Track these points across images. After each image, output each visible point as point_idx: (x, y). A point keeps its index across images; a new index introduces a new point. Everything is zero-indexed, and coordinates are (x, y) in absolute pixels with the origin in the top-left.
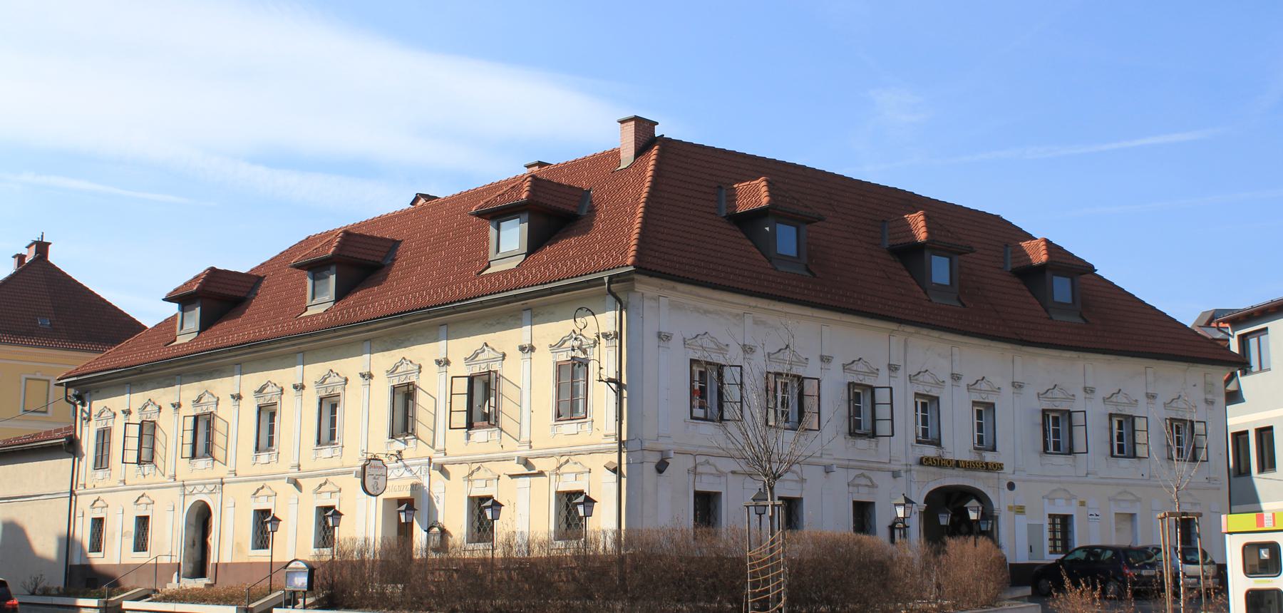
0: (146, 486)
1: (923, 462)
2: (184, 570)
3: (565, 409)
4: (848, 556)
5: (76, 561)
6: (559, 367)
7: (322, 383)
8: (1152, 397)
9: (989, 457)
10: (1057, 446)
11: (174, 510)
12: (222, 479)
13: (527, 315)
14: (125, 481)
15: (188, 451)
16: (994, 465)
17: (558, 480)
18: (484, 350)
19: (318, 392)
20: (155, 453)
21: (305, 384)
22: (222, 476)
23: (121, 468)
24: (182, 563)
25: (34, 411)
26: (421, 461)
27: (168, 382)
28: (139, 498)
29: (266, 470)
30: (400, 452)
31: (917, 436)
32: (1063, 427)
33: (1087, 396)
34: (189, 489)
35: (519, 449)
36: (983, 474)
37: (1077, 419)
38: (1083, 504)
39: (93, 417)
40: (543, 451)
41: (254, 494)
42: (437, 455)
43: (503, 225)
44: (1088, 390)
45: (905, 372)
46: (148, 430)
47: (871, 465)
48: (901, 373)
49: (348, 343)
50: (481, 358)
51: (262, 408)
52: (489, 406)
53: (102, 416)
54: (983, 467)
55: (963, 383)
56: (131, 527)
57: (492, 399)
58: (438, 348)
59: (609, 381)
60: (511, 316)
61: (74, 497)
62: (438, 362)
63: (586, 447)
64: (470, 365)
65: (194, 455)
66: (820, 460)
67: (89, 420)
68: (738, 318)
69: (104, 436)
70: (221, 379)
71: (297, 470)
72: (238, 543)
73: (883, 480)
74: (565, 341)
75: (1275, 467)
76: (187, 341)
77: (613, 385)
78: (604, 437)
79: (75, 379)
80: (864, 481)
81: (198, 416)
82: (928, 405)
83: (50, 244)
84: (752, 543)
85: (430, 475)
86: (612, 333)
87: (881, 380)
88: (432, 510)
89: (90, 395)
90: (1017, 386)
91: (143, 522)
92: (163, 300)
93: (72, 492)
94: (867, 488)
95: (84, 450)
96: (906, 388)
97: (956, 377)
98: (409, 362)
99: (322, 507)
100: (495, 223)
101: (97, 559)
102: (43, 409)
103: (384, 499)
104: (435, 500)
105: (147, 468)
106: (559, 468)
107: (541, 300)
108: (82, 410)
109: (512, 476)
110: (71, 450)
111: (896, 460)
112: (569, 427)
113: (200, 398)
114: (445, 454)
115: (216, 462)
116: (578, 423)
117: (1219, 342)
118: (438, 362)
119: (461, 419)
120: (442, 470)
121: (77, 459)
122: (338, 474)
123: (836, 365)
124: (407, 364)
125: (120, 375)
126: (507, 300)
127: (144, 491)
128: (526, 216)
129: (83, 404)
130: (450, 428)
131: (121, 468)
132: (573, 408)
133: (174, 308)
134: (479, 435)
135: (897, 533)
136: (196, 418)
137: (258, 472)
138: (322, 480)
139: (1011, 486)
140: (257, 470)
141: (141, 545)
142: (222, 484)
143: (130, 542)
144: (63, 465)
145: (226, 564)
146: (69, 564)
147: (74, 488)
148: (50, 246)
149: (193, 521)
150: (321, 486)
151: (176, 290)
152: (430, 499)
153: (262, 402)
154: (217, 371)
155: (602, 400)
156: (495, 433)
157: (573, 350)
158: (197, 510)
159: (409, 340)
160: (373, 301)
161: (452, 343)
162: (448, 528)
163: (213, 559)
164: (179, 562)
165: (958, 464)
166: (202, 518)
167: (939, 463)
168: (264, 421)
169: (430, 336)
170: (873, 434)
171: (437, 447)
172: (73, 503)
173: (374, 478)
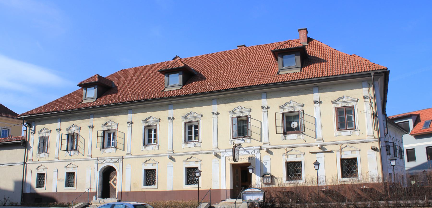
0: (73, 160)
2: (99, 195)
4: (296, 186)
5: (28, 191)
7: (186, 117)
11: (91, 170)
12: (123, 157)
13: (316, 89)
14: (58, 158)
15: (100, 145)
17: (341, 154)
18: (291, 103)
19: (39, 135)
20: (78, 147)
21: (61, 129)
22: (123, 155)
24: (98, 192)
26: (254, 148)
27: (85, 117)
28: (68, 165)
29: (151, 153)
34: (100, 161)
35: (316, 142)
39: (36, 132)
40: (332, 142)
41: (144, 163)
42: (264, 145)
43: (88, 89)
49: (202, 100)
50: (289, 106)
51: (146, 127)
53: (42, 131)
58: (57, 125)
60: (306, 89)
61: (25, 165)
62: (57, 130)
63: (357, 141)
64: (231, 114)
65: (103, 147)
67: (35, 133)
70: (119, 116)
71: (172, 152)
72: (134, 184)
74: (340, 99)
75: (416, 160)
76: (93, 101)
79: (29, 116)
81: (105, 131)
84: (395, 179)
85: (260, 153)
86: (216, 112)
88: (262, 166)
89: (35, 123)
92: (77, 85)
93: (25, 163)
95: (31, 145)
98: (76, 126)
99: (39, 173)
100: (167, 75)
101: (40, 190)
104: (264, 164)
105: (73, 153)
106: (341, 149)
107: (323, 83)
108: (30, 130)
109: (312, 153)
110: (25, 145)
113: (106, 123)
114: (270, 145)
115: (305, 135)
116: (351, 131)
117: (398, 124)
118: (57, 130)
120: (268, 151)
121: (27, 149)
122: (199, 154)
124: (46, 130)
125: (38, 117)
126: (319, 81)
127: (42, 164)
128: (96, 86)
129: (31, 127)
130: (61, 150)
133: (79, 88)
137: (146, 154)
138: (190, 156)
140: (145, 152)
142: (123, 158)
144: (21, 152)
145: (128, 192)
146: (23, 192)
147: (25, 161)
150: (188, 159)
151: (83, 82)
152: (261, 164)
154: (116, 112)
156: (301, 136)
158: (104, 169)
159: (242, 99)
160: (109, 99)
161: (321, 94)
162: (273, 174)
164: (96, 191)
168: (146, 133)
169: (126, 112)
171: (263, 141)
172: (25, 167)
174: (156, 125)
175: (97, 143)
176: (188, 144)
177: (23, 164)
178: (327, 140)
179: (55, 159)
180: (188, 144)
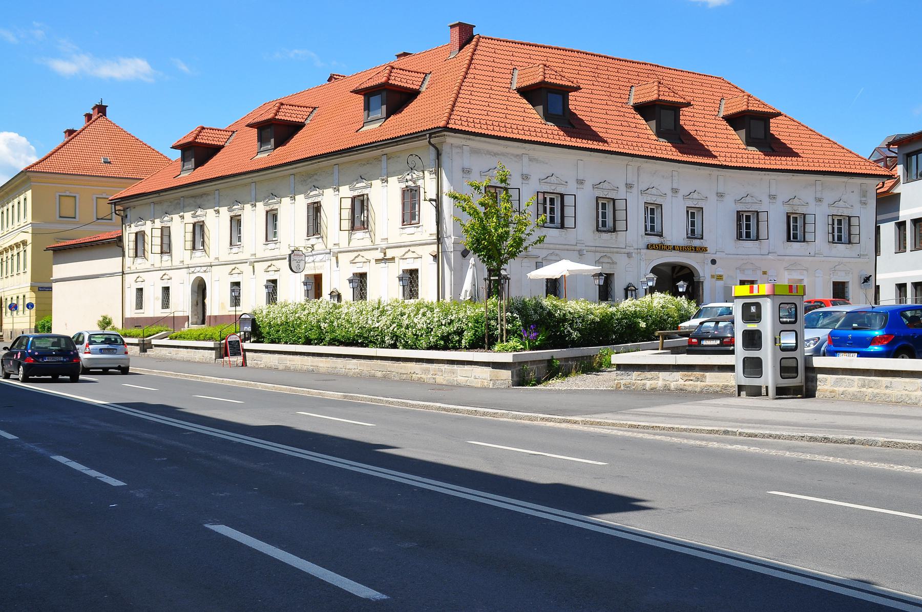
1: (650, 247)
3: (407, 217)
6: (404, 192)
8: (819, 200)
9: (696, 243)
10: (748, 235)
16: (701, 248)
23: (154, 258)
25: (102, 219)
30: (313, 246)
31: (646, 230)
32: (753, 223)
33: (771, 201)
36: (693, 254)
37: (763, 217)
38: (765, 273)
44: (772, 197)
45: (638, 188)
46: (166, 233)
47: (612, 249)
48: (635, 190)
52: (364, 217)
54: (692, 250)
55: (680, 195)
56: (159, 293)
57: (365, 212)
59: (431, 200)
65: (136, 256)
66: (576, 247)
68: (518, 157)
69: (140, 237)
73: (622, 260)
77: (434, 203)
78: (429, 235)
80: (606, 260)
82: (652, 211)
83: (107, 106)
87: (621, 194)
90: (720, 195)
91: (166, 290)
94: (609, 264)
96: (638, 198)
97: (675, 191)
102: (109, 217)
103: (305, 275)
111: (630, 247)
112: (411, 230)
119: (346, 225)
122: (278, 259)
123: (588, 185)
131: (154, 258)
132: (413, 217)
134: (359, 234)
135: (629, 293)
136: (194, 225)
139: (714, 262)
141: (166, 304)
143: (159, 303)
148: (107, 108)
149: (196, 289)
153: (232, 214)
155: (427, 211)
157: (407, 181)
163: (208, 313)
165: (674, 248)
166: (200, 289)
167: (661, 247)
170: (614, 230)
173: (297, 262)
174: (240, 215)
175: (519, 198)
176: (406, 228)
177: (121, 274)
178: (393, 241)
179: (382, 243)
180: (406, 228)
